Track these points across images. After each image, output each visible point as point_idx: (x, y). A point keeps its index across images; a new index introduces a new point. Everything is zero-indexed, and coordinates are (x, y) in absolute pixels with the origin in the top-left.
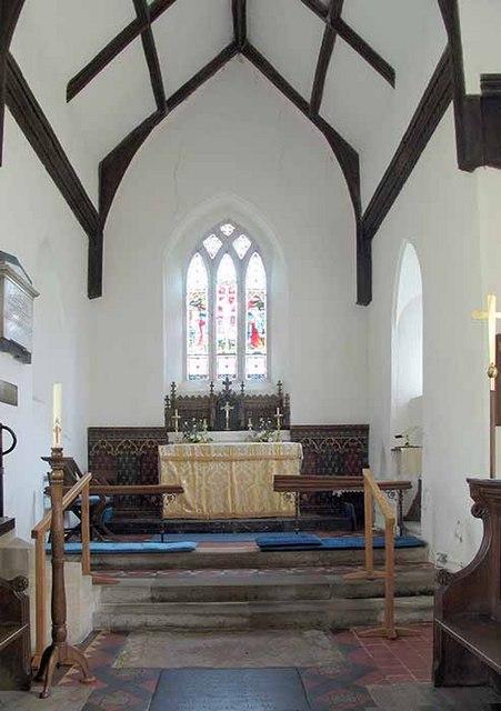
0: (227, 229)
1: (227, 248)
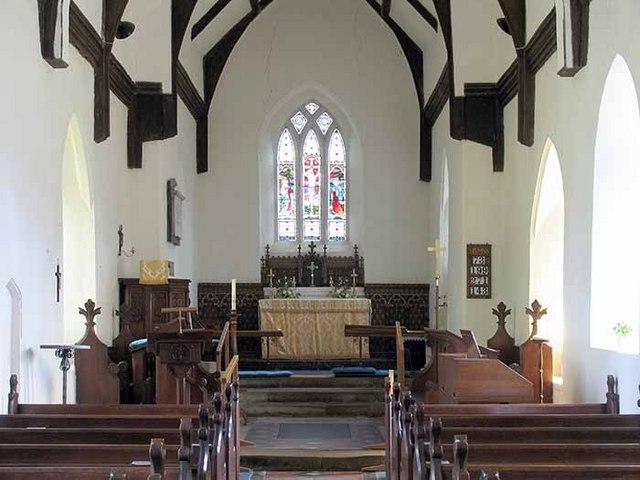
0: (312, 108)
1: (312, 123)
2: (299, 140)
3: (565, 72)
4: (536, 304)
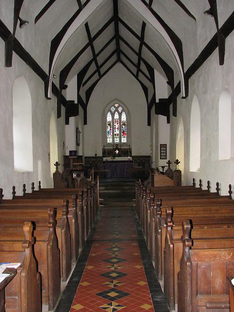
0: (116, 105)
1: (117, 110)
2: (113, 115)
3: (183, 98)
4: (177, 160)
